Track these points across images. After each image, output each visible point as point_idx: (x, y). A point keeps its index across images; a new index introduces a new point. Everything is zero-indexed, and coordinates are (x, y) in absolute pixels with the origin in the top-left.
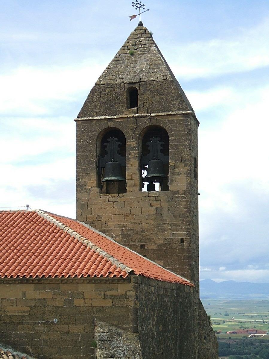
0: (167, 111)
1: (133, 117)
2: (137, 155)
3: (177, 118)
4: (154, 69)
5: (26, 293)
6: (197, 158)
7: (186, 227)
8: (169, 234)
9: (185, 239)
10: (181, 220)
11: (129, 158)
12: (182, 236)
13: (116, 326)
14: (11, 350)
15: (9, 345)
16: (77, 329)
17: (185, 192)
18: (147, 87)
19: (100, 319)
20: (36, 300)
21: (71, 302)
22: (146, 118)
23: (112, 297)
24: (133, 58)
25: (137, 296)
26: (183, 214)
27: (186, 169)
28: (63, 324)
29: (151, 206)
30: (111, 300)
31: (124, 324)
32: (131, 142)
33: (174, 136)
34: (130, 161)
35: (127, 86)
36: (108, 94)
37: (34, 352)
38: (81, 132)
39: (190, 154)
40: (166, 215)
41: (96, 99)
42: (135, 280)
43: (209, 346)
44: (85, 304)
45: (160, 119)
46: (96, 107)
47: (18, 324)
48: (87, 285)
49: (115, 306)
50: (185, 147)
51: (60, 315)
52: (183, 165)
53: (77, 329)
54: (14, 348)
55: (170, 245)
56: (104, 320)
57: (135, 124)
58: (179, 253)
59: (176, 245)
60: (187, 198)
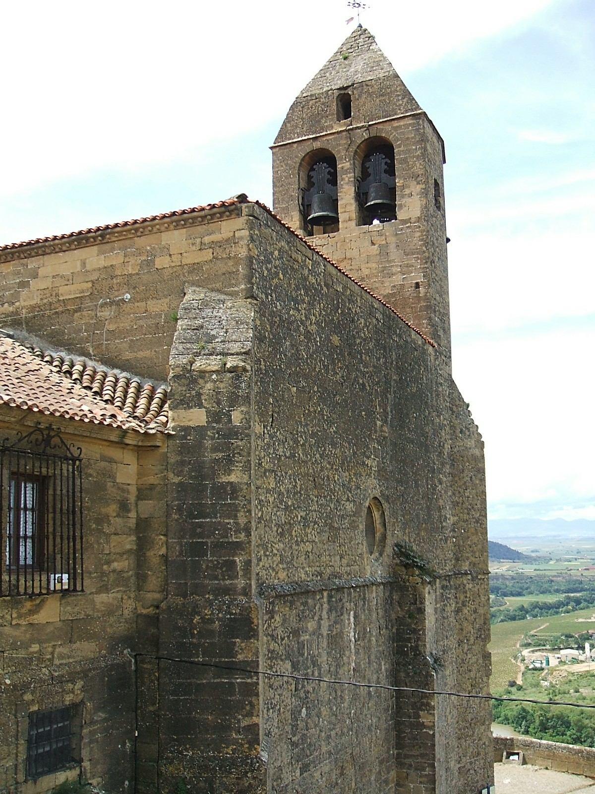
0: (390, 116)
1: (346, 130)
2: (352, 179)
3: (405, 123)
4: (373, 67)
5: (87, 261)
6: (443, 183)
7: (422, 266)
8: (398, 279)
9: (421, 284)
10: (414, 258)
11: (342, 185)
12: (417, 280)
13: (219, 291)
14: (64, 353)
15: (61, 347)
16: (158, 305)
17: (419, 219)
18: (362, 90)
19: (193, 284)
20: (99, 269)
21: (150, 263)
22: (362, 130)
23: (213, 245)
24: (346, 62)
25: (252, 237)
26: (417, 249)
27: (419, 188)
28: (138, 302)
29: (373, 244)
30: (211, 250)
31: (232, 285)
32: (344, 163)
33: (400, 147)
34: (343, 188)
35: (336, 93)
36: (312, 108)
37: (96, 353)
38: (278, 162)
39: (425, 167)
40: (395, 254)
41: (298, 117)
42: (249, 211)
43: (469, 443)
44: (171, 264)
45: (382, 127)
46: (297, 127)
47: (76, 311)
48: (176, 232)
49: (217, 258)
50: (417, 158)
51: (134, 288)
52: (415, 183)
53: (159, 306)
54: (68, 350)
55: (401, 294)
56: (200, 284)
57: (349, 140)
58: (413, 304)
59: (408, 293)
60: (421, 226)
